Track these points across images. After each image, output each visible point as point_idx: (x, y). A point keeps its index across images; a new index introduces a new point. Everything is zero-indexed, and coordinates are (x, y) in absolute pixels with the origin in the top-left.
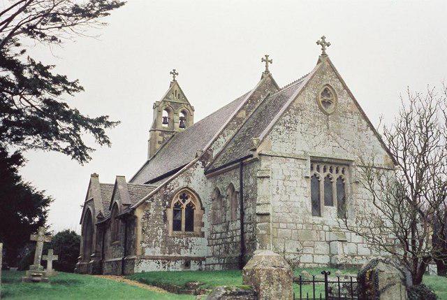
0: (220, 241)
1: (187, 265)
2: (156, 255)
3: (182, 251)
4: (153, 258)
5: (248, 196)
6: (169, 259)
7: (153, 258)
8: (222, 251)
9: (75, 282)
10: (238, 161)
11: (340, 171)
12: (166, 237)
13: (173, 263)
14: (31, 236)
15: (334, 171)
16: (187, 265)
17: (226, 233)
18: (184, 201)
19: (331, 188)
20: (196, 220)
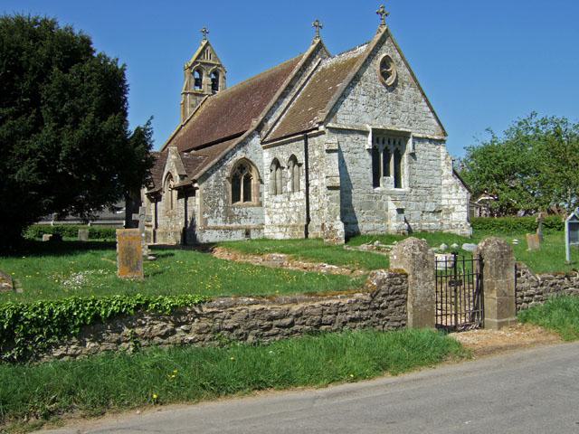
0: (281, 211)
1: (247, 233)
2: (219, 225)
3: (242, 221)
4: (215, 228)
5: (312, 168)
6: (231, 229)
7: (215, 228)
8: (283, 220)
9: (172, 255)
10: (302, 133)
11: (386, 142)
12: (226, 208)
13: (234, 232)
14: (133, 215)
15: (392, 142)
16: (247, 233)
17: (287, 203)
18: (242, 172)
19: (212, 167)
20: (253, 190)
